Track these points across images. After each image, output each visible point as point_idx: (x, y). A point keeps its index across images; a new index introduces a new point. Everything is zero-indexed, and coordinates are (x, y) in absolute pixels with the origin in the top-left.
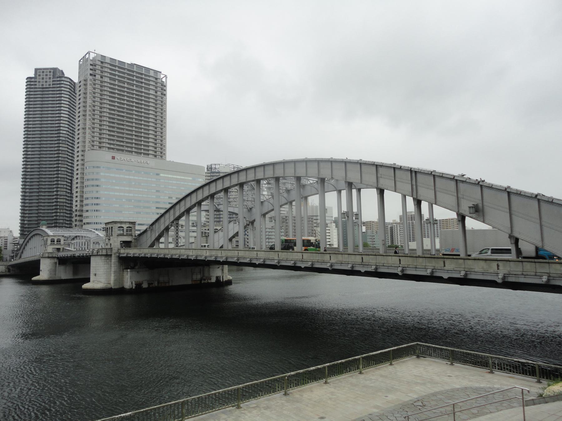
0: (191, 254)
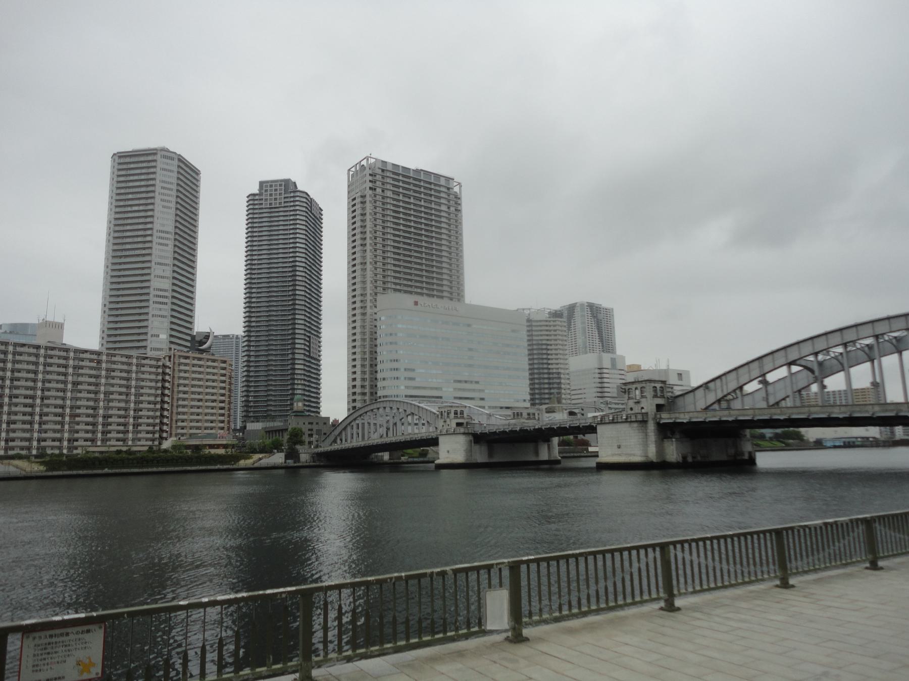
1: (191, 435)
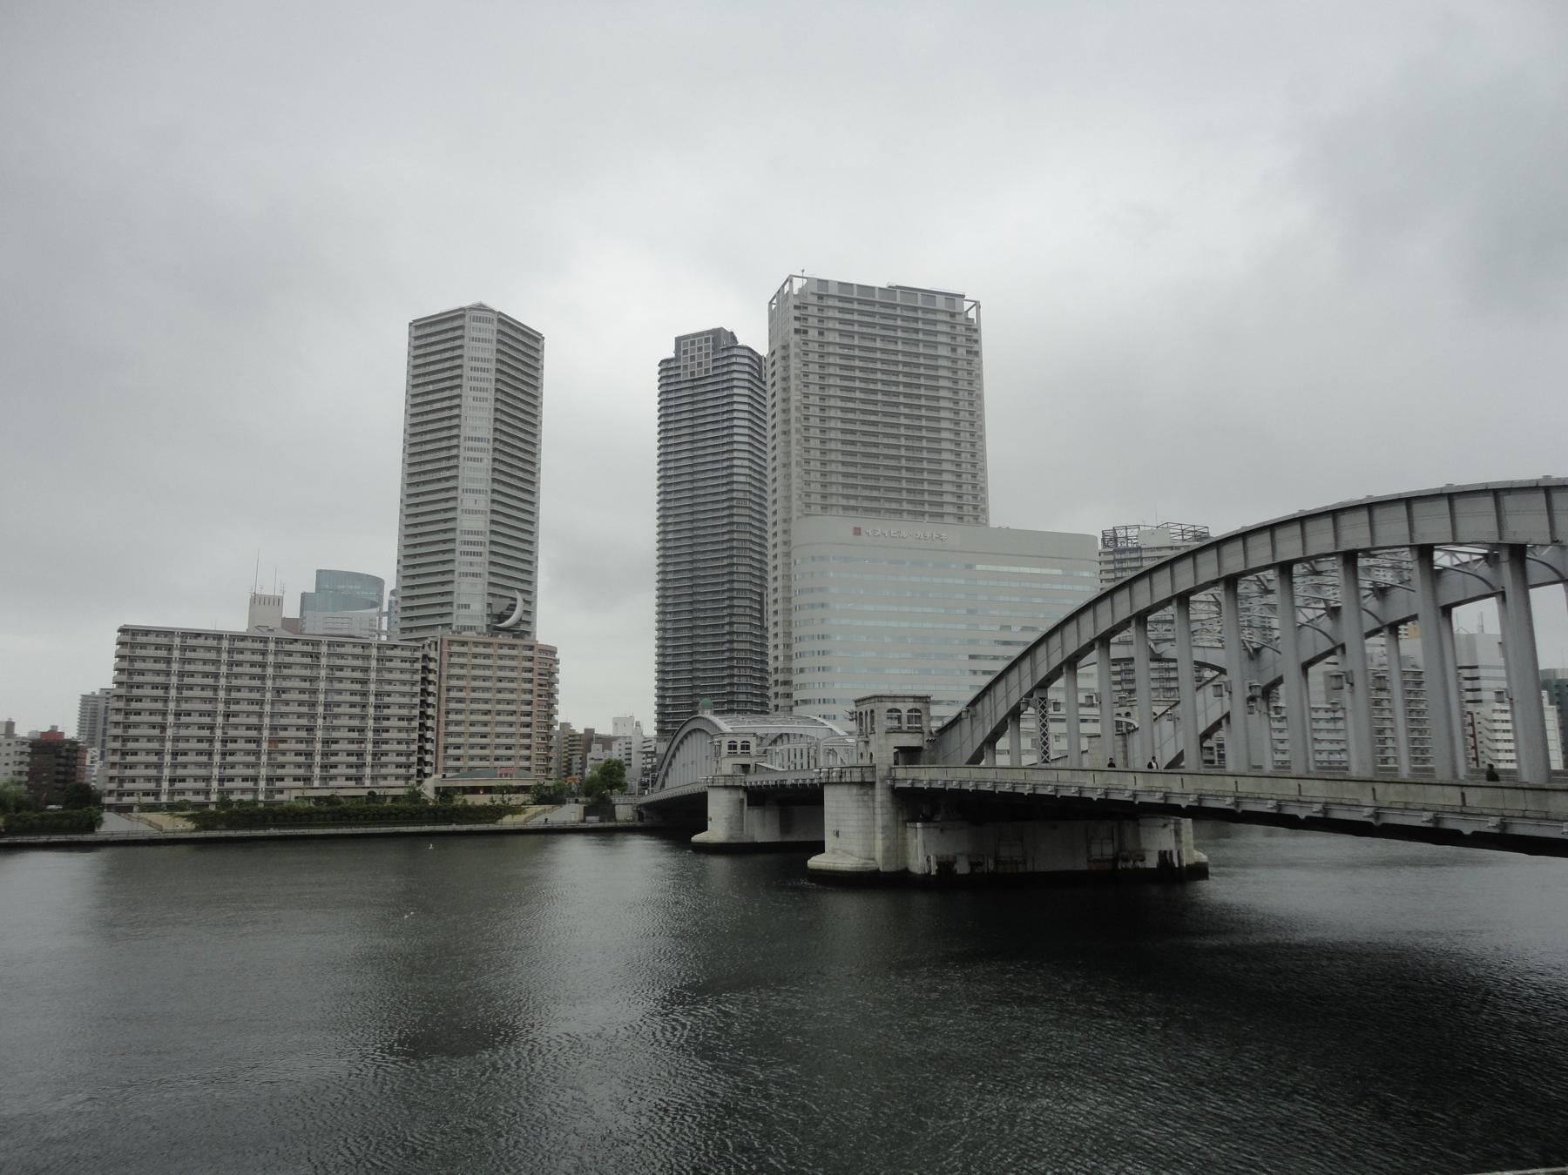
0: (1089, 783)
1: (471, 769)
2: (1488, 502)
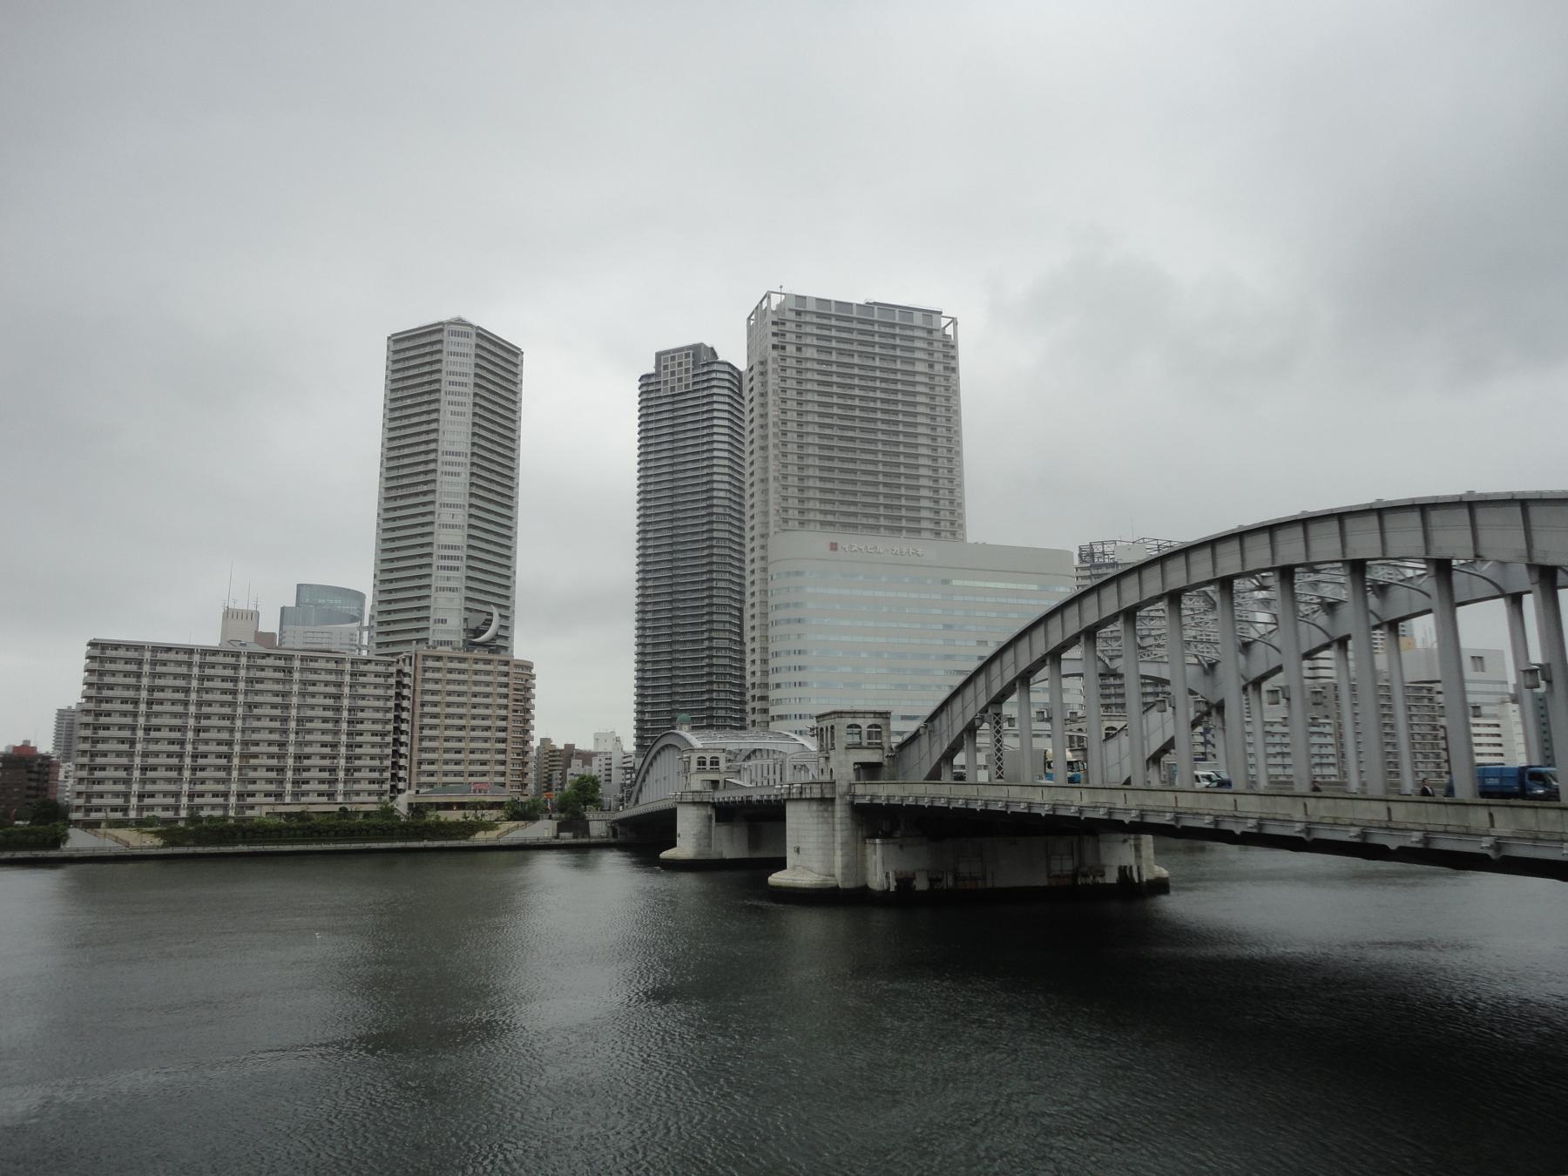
0: (1038, 799)
1: (445, 784)
2: (1415, 518)
